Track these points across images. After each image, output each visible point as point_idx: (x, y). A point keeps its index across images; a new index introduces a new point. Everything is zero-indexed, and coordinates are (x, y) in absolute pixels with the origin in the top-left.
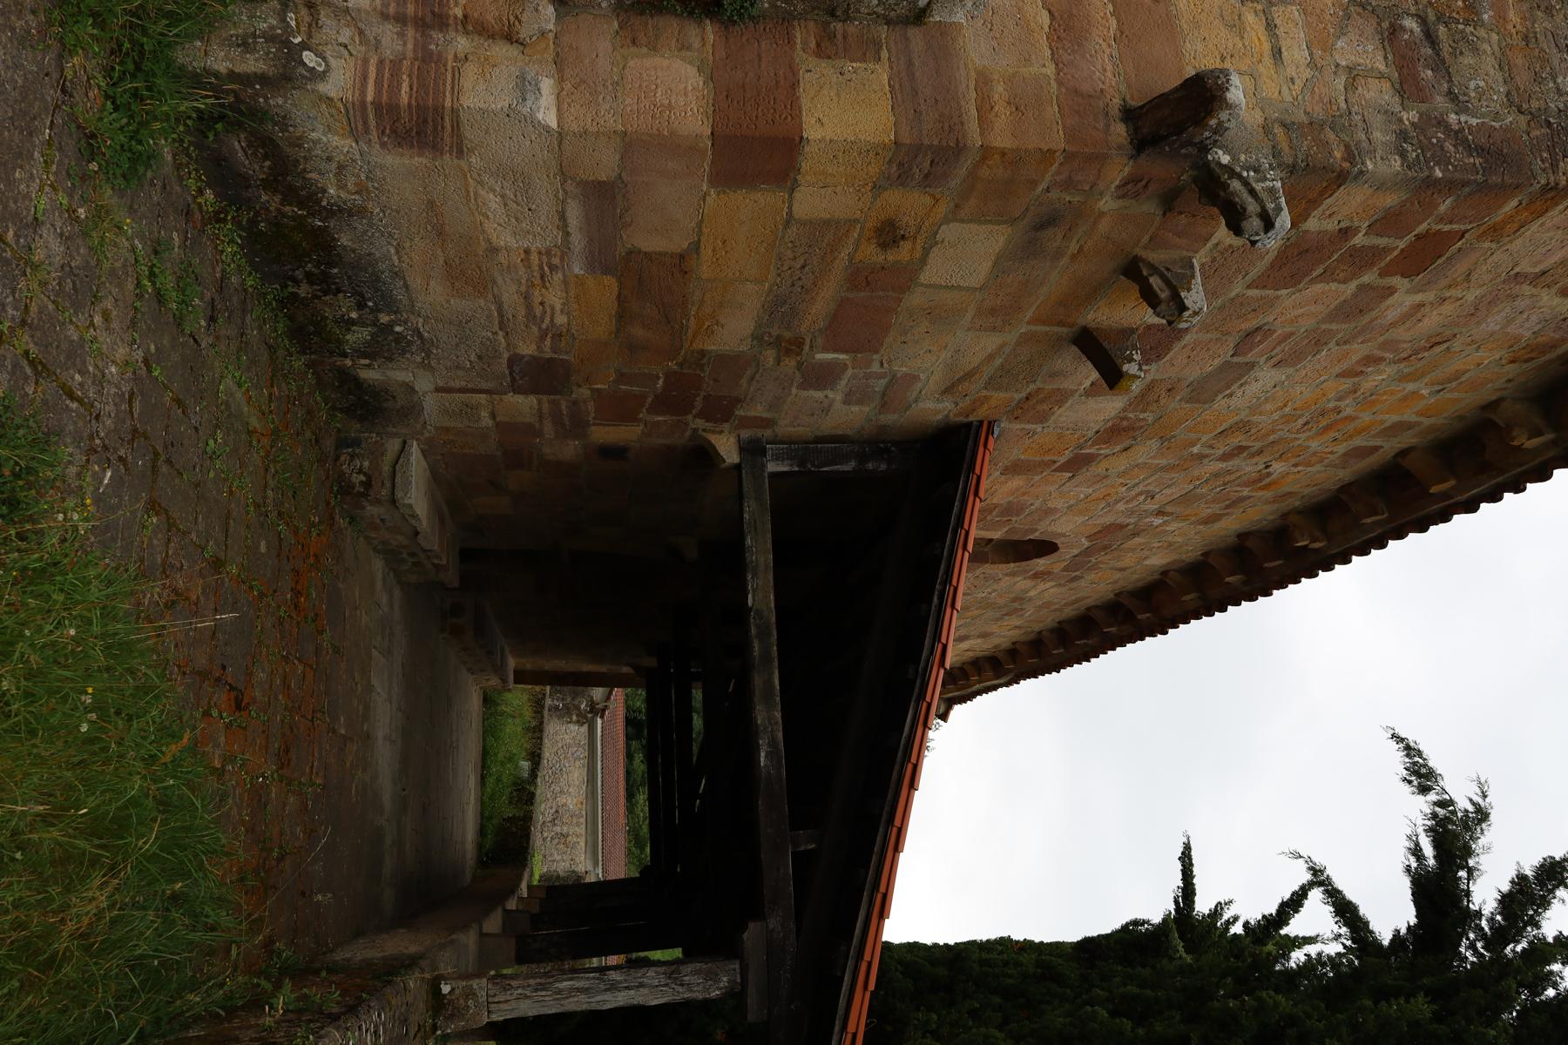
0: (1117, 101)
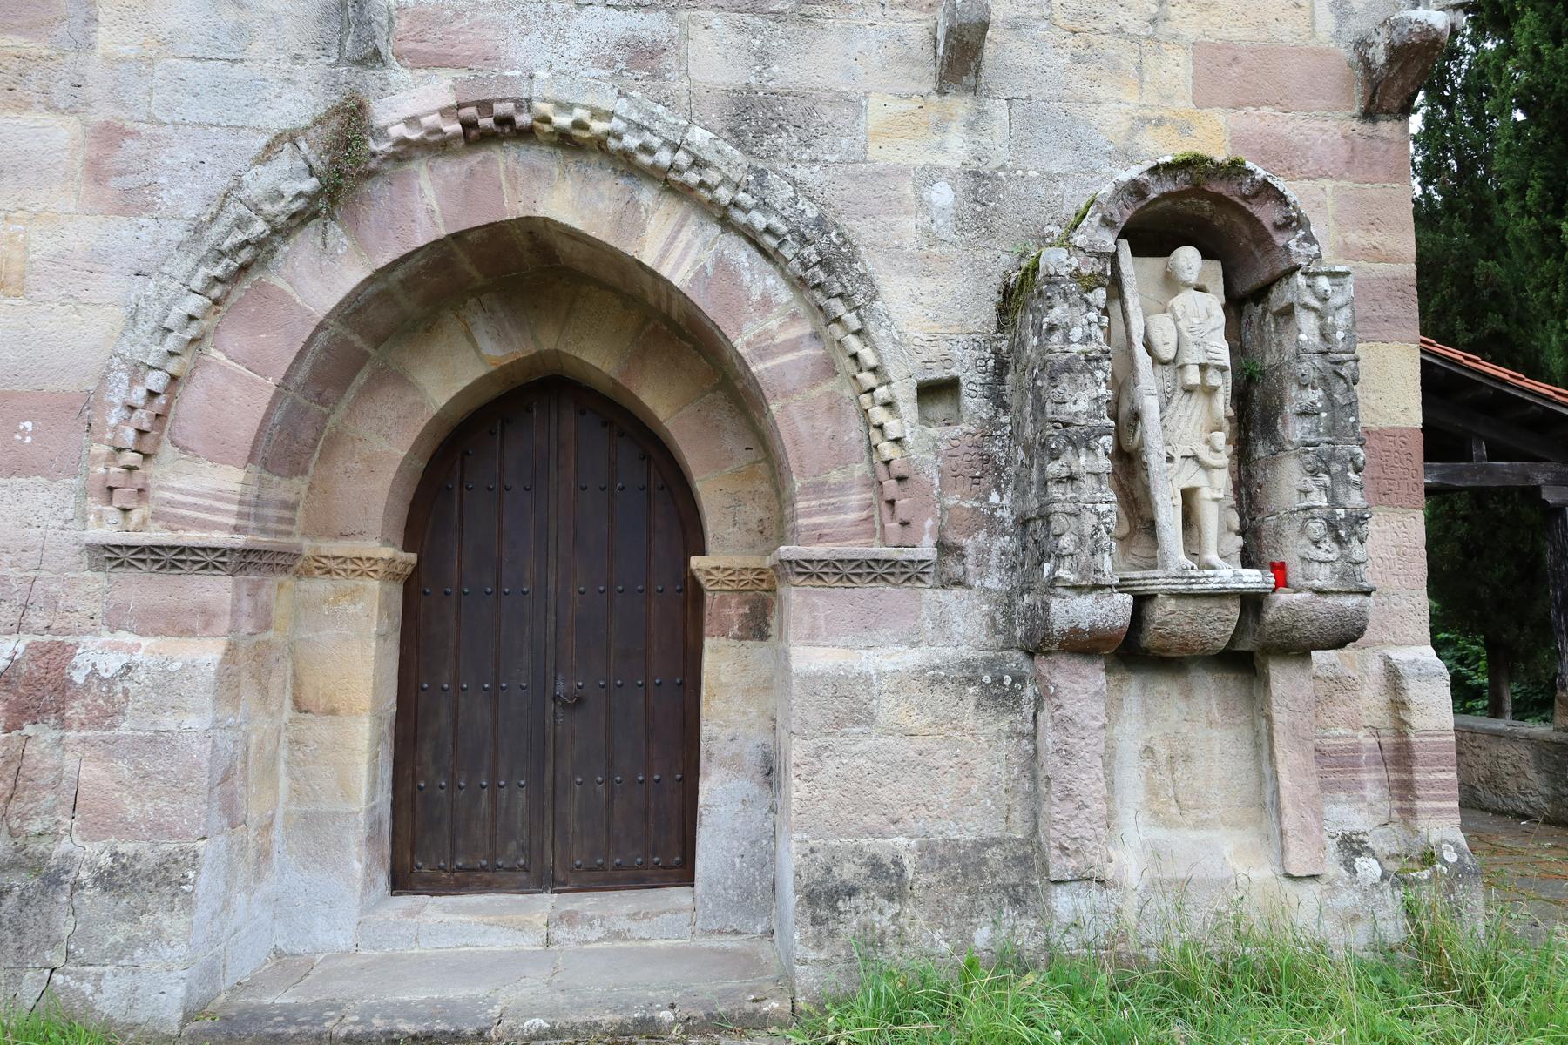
0: (1355, 124)
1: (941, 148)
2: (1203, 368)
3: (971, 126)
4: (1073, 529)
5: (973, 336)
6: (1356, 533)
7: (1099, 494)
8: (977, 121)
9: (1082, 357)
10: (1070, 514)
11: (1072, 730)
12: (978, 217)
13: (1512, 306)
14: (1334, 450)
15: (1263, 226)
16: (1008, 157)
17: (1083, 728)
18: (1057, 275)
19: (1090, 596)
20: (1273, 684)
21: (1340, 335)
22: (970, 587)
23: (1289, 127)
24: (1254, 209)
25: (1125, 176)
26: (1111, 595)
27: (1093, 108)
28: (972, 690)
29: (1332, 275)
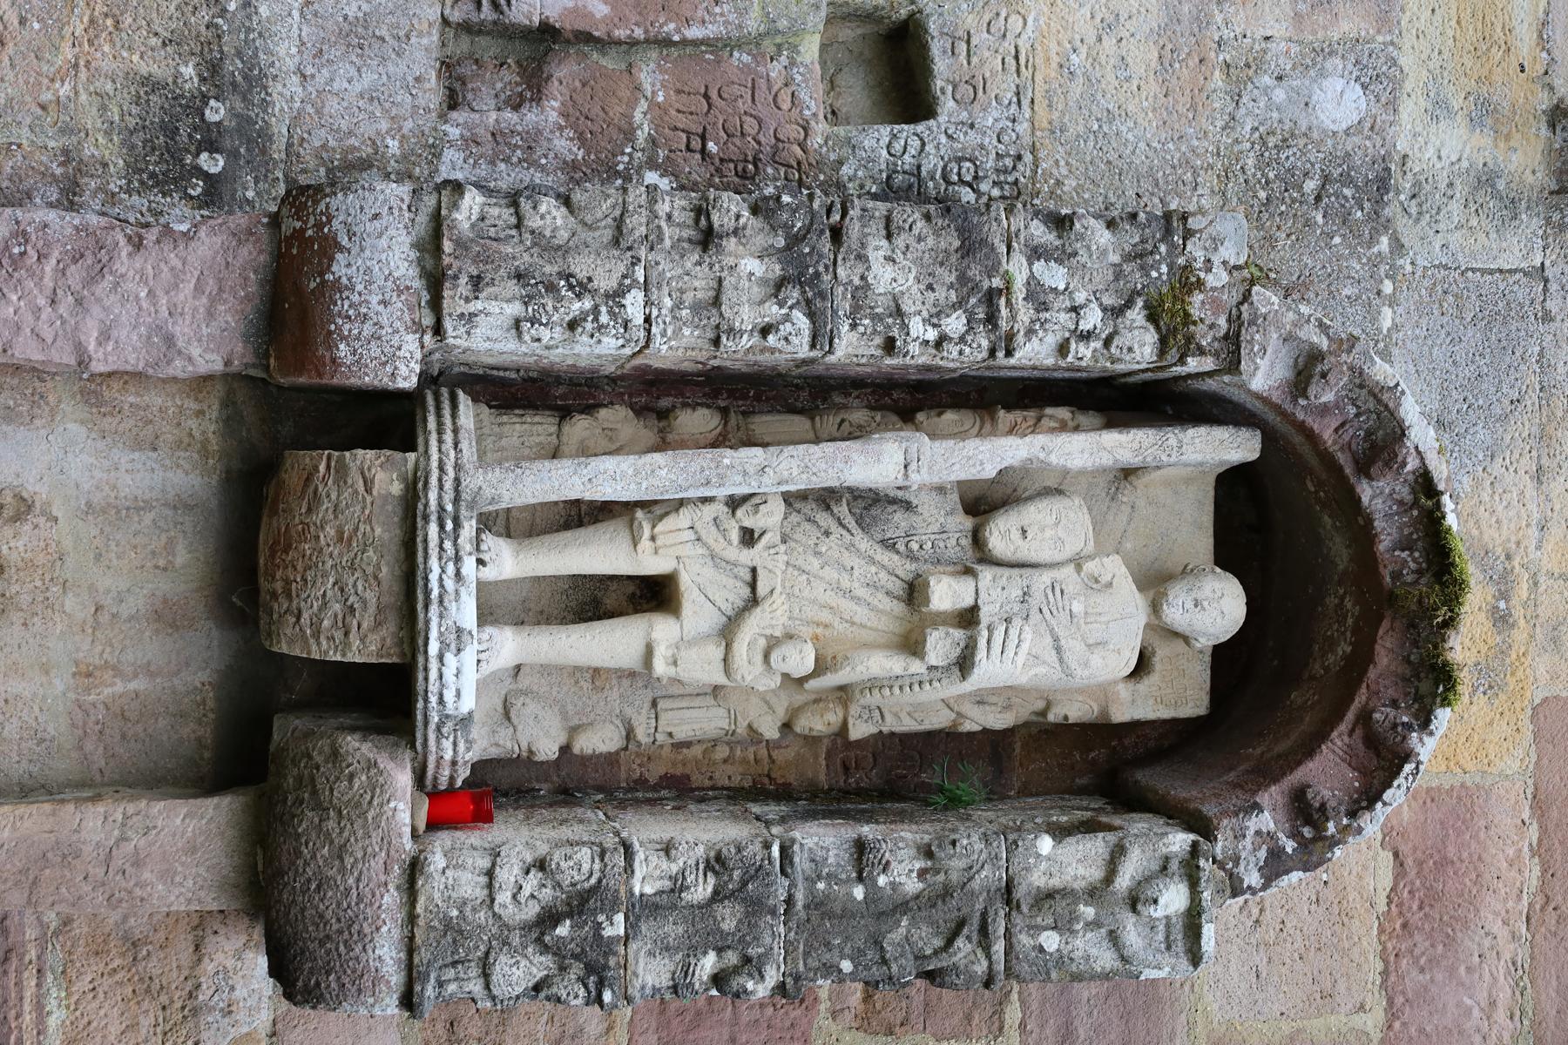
1: (1438, 109)
3: (1485, 180)
4: (585, 235)
5: (1028, 158)
6: (563, 969)
7: (668, 302)
8: (1496, 195)
9: (997, 282)
10: (619, 224)
11: (75, 274)
12: (1291, 181)
13: (1254, 749)
14: (773, 912)
15: (1299, 763)
16: (1421, 262)
17: (79, 302)
18: (1188, 234)
19: (413, 272)
20: (182, 807)
21: (1051, 941)
22: (443, 117)
23: (1497, 927)
24: (1340, 738)
25: (1410, 411)
26: (418, 328)
27: (1527, 463)
28: (188, 71)
29: (1192, 921)
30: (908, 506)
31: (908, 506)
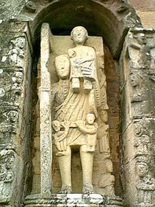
2: (81, 79)
30: (57, 93)
31: (57, 93)
